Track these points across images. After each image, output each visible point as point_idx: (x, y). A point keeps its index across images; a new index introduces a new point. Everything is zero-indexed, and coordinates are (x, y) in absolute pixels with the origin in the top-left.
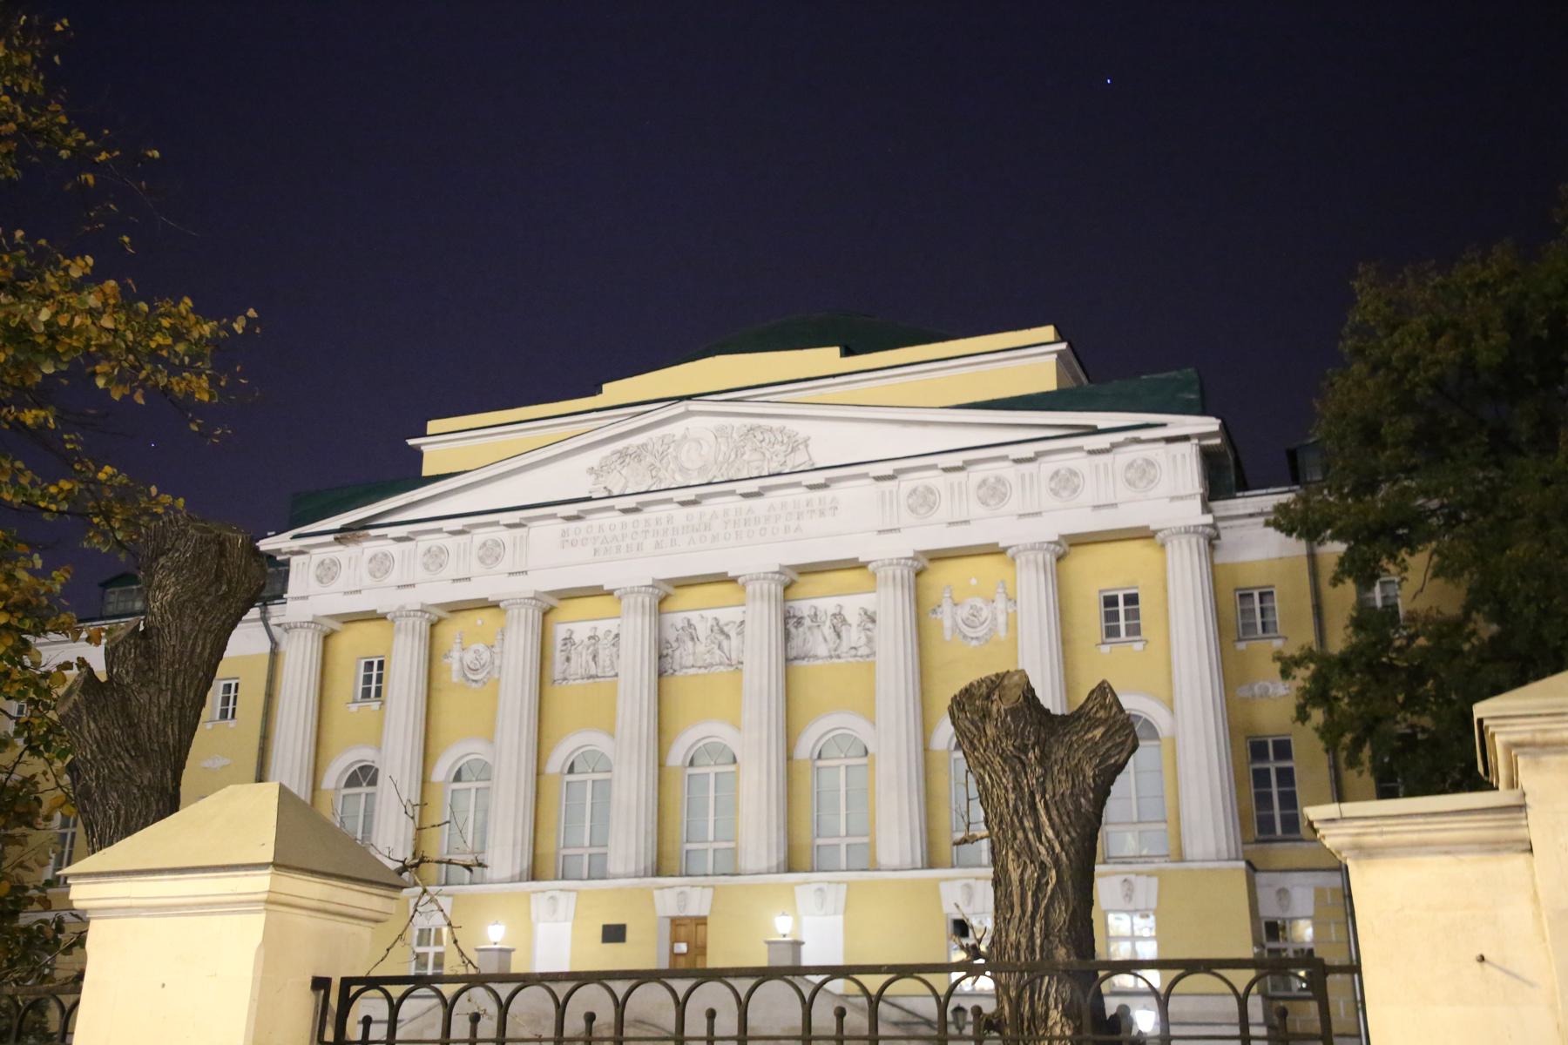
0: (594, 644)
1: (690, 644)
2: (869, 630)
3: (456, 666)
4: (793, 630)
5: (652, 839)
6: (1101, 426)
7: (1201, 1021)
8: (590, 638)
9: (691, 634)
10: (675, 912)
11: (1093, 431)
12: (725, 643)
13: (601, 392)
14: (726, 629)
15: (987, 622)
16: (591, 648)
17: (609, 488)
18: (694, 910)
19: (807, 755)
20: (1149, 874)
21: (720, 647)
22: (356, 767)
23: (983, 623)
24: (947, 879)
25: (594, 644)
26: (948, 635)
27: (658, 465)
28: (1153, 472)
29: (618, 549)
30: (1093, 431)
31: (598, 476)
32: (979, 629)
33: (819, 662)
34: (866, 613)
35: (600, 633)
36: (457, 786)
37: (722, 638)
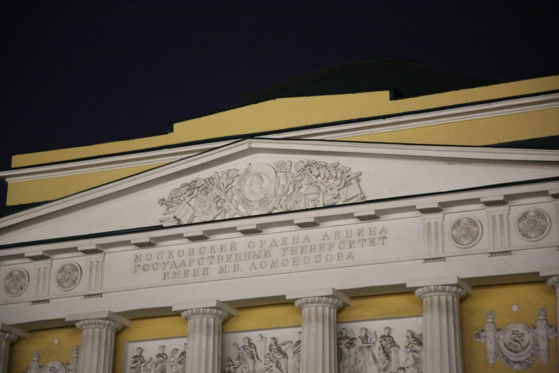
0: (162, 362)
1: (250, 362)
2: (415, 351)
3: (491, 347)
8: (158, 356)
9: (251, 353)
12: (283, 361)
14: (283, 348)
15: (529, 347)
16: (159, 366)
21: (278, 366)
23: (527, 347)
25: (162, 362)
27: (223, 197)
29: (186, 273)
32: (520, 354)
34: (413, 336)
35: (168, 352)
37: (279, 356)
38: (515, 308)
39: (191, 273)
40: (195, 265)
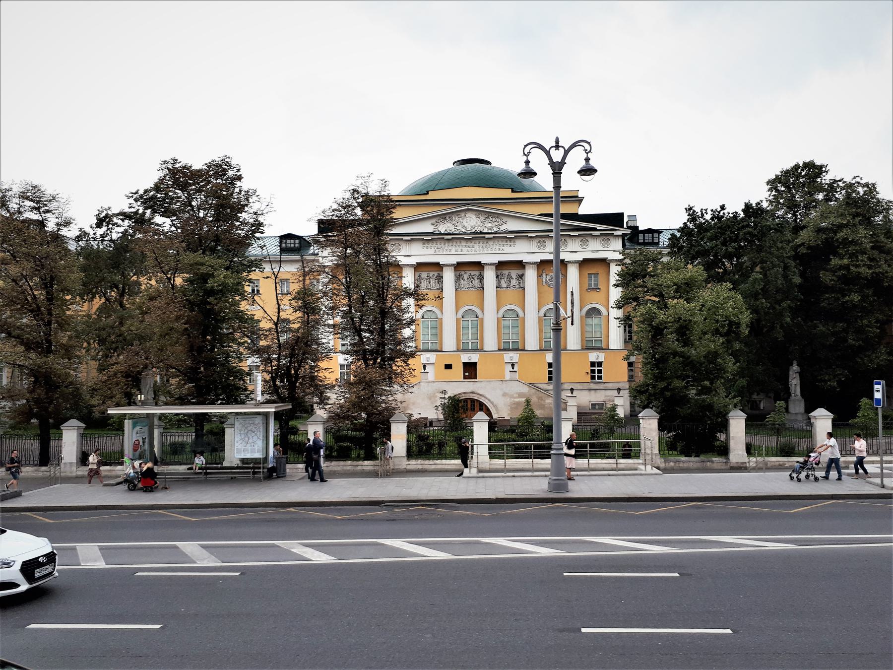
6: (598, 228)
40: (446, 248)
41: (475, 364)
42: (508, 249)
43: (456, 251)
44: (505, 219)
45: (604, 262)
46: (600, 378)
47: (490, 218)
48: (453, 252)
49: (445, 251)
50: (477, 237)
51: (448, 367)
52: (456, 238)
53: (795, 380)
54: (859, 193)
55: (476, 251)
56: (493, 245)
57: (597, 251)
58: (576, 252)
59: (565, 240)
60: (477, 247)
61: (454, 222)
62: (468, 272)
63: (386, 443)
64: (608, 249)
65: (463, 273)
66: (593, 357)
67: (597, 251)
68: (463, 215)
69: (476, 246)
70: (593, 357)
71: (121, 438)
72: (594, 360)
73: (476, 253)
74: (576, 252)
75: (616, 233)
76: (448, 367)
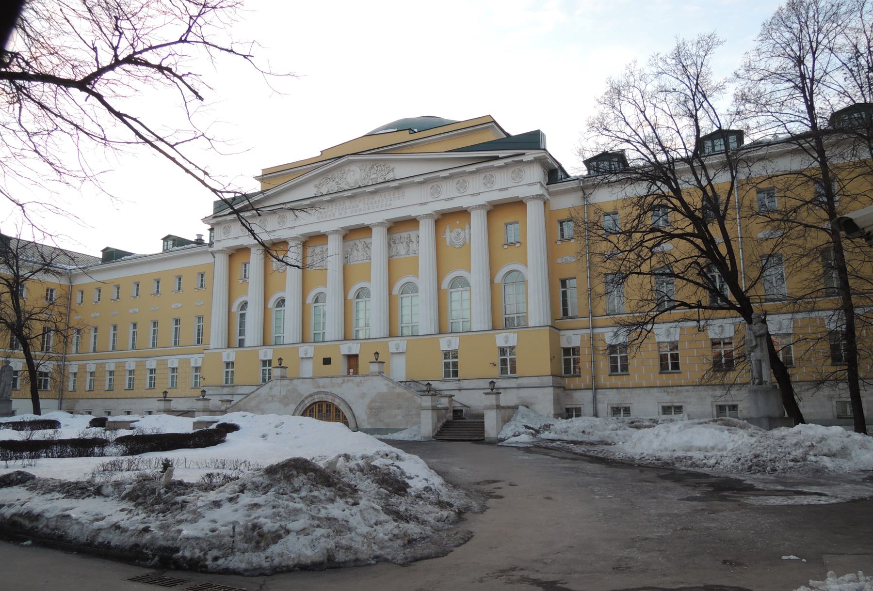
4: (392, 245)
5: (386, 324)
6: (500, 156)
7: (530, 386)
10: (347, 353)
11: (497, 158)
13: (103, 251)
17: (724, 43)
18: (353, 352)
19: (500, 282)
20: (514, 333)
22: (279, 300)
24: (441, 338)
26: (448, 244)
28: (522, 174)
29: (326, 216)
30: (497, 158)
31: (318, 188)
33: (402, 257)
36: (357, 300)
37: (366, 249)
38: (458, 222)
39: (328, 216)
40: (330, 213)
41: (356, 356)
42: (396, 203)
43: (340, 214)
44: (392, 165)
45: (519, 204)
46: (513, 370)
47: (375, 167)
48: (337, 216)
49: (328, 216)
50: (356, 193)
51: (327, 361)
52: (335, 198)
53: (758, 350)
54: (844, 45)
55: (360, 210)
56: (379, 201)
57: (506, 189)
58: (478, 194)
59: (438, 185)
60: (362, 204)
61: (337, 180)
62: (362, 241)
63: (293, 558)
64: (520, 184)
65: (357, 242)
66: (502, 339)
67: (506, 189)
68: (347, 169)
69: (361, 205)
70: (502, 339)
71: (166, 247)
72: (503, 344)
73: (323, 220)
74: (478, 194)
75: (525, 158)
76: (327, 361)
